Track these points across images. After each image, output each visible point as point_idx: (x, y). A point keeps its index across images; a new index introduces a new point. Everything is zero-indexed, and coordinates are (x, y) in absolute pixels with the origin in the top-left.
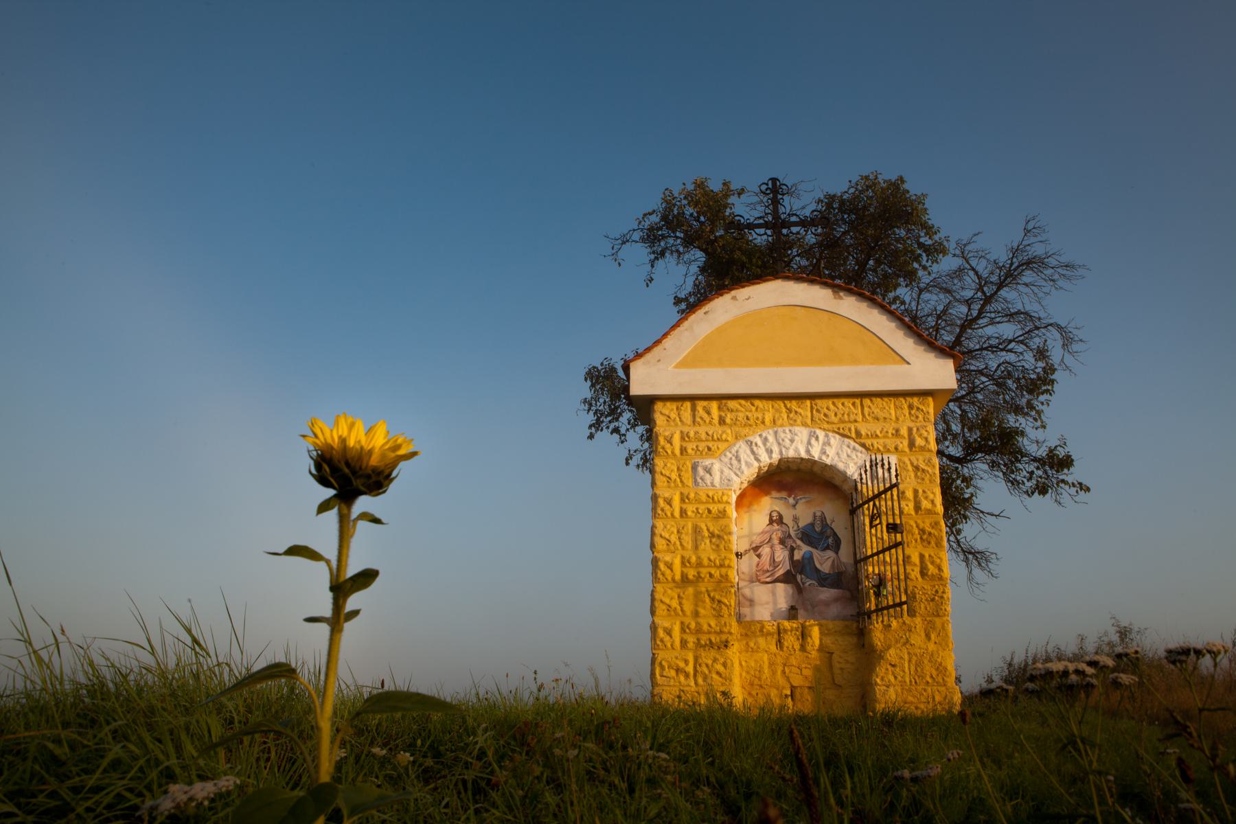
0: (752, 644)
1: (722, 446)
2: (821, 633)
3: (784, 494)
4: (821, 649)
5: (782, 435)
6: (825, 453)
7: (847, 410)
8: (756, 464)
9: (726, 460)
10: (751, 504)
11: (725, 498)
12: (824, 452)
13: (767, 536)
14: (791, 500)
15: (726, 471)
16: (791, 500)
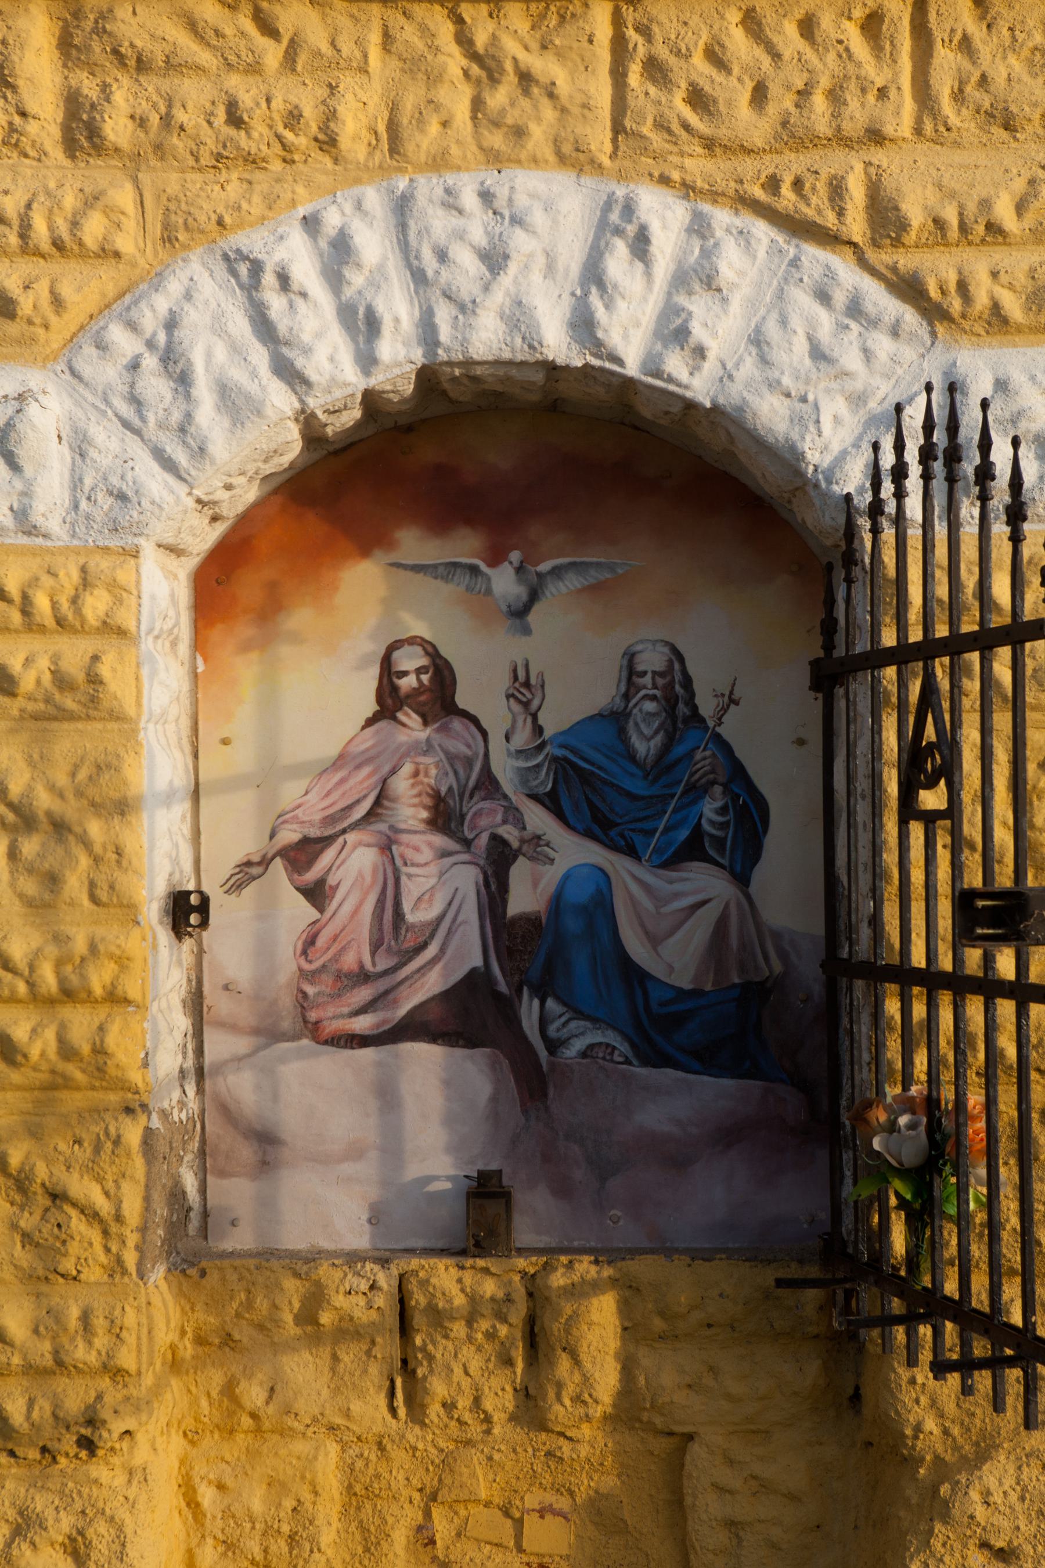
0: (254, 1394)
1: (83, 287)
2: (632, 1330)
3: (464, 546)
4: (630, 1411)
5: (440, 224)
6: (680, 335)
7: (827, 68)
8: (281, 400)
9: (107, 373)
10: (270, 610)
11: (96, 605)
12: (674, 331)
13: (361, 784)
14: (504, 582)
15: (107, 440)
16: (504, 582)
